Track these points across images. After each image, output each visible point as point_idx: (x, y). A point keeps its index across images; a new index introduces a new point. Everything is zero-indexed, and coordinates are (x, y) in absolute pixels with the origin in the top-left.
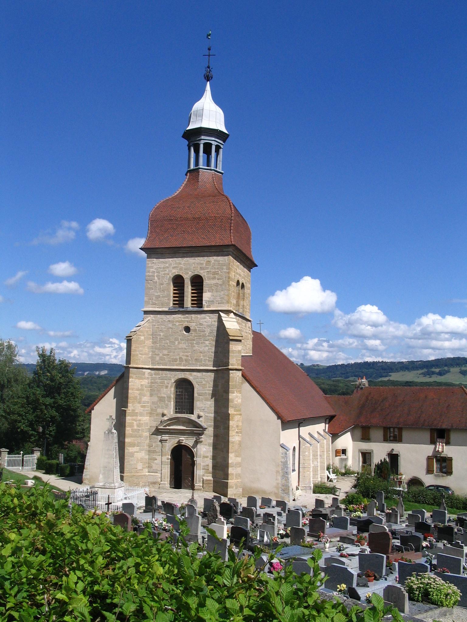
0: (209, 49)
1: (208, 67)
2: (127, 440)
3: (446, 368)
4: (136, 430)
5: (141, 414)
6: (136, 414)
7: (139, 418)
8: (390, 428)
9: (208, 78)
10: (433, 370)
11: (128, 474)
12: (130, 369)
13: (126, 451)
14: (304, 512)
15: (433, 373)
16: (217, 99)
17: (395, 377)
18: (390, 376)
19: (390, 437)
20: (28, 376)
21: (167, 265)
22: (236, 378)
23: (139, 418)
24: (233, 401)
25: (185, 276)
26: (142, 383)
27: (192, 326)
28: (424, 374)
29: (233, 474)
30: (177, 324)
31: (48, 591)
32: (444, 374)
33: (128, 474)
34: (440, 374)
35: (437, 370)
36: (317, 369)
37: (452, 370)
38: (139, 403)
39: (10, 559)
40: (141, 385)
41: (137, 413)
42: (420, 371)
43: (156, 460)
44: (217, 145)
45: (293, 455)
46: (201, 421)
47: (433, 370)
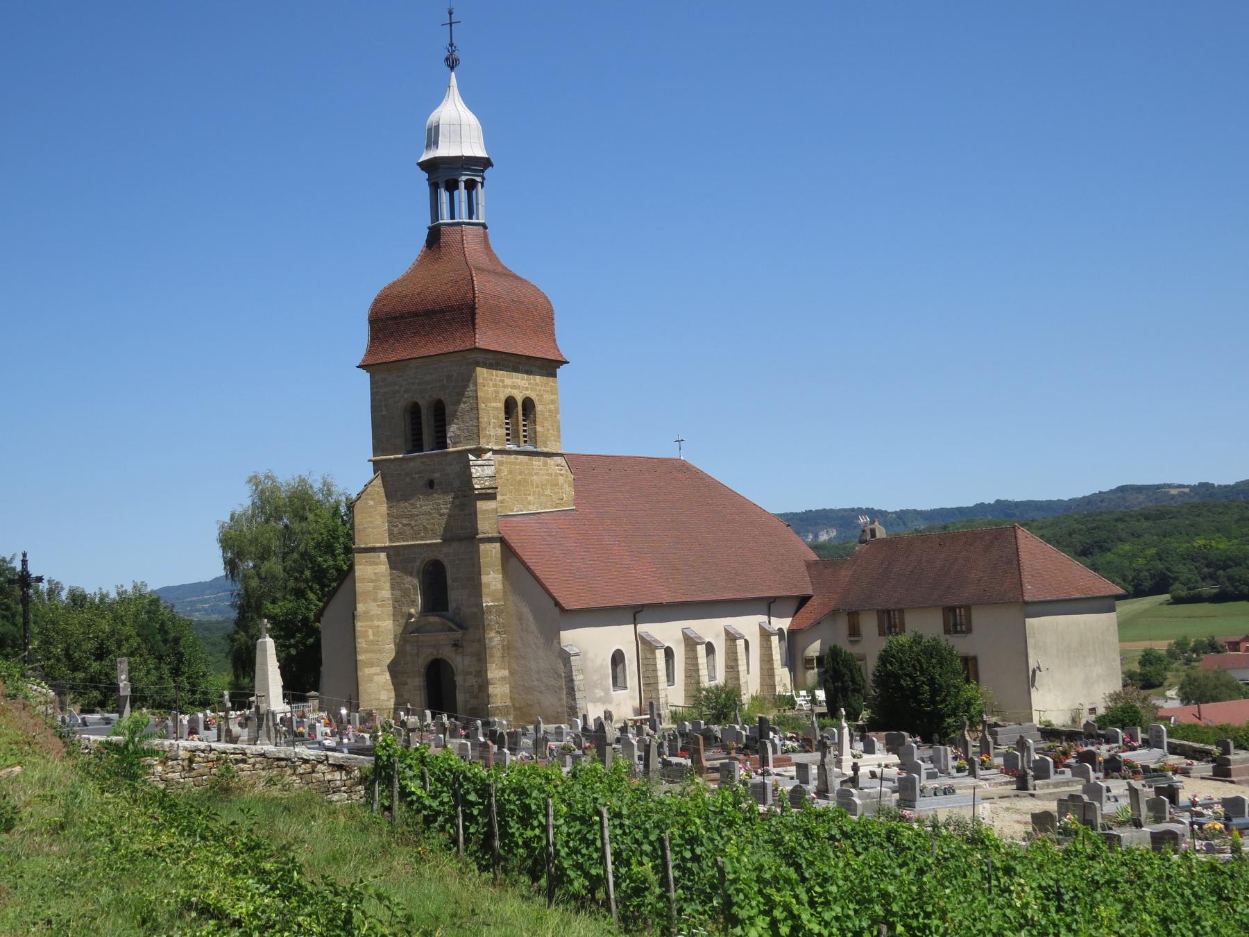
0: (451, 13)
1: (451, 45)
2: (359, 658)
4: (372, 641)
7: (376, 623)
8: (888, 612)
9: (452, 63)
11: (1235, 767)
12: (482, 547)
13: (360, 674)
14: (310, 704)
19: (890, 628)
21: (397, 388)
22: (491, 551)
23: (376, 623)
24: (488, 585)
25: (422, 403)
26: (376, 571)
27: (437, 475)
29: (496, 695)
30: (417, 476)
33: (1235, 767)
38: (375, 600)
39: (921, 920)
40: (375, 573)
41: (373, 615)
43: (407, 684)
44: (467, 180)
45: (727, 667)
46: (717, 636)
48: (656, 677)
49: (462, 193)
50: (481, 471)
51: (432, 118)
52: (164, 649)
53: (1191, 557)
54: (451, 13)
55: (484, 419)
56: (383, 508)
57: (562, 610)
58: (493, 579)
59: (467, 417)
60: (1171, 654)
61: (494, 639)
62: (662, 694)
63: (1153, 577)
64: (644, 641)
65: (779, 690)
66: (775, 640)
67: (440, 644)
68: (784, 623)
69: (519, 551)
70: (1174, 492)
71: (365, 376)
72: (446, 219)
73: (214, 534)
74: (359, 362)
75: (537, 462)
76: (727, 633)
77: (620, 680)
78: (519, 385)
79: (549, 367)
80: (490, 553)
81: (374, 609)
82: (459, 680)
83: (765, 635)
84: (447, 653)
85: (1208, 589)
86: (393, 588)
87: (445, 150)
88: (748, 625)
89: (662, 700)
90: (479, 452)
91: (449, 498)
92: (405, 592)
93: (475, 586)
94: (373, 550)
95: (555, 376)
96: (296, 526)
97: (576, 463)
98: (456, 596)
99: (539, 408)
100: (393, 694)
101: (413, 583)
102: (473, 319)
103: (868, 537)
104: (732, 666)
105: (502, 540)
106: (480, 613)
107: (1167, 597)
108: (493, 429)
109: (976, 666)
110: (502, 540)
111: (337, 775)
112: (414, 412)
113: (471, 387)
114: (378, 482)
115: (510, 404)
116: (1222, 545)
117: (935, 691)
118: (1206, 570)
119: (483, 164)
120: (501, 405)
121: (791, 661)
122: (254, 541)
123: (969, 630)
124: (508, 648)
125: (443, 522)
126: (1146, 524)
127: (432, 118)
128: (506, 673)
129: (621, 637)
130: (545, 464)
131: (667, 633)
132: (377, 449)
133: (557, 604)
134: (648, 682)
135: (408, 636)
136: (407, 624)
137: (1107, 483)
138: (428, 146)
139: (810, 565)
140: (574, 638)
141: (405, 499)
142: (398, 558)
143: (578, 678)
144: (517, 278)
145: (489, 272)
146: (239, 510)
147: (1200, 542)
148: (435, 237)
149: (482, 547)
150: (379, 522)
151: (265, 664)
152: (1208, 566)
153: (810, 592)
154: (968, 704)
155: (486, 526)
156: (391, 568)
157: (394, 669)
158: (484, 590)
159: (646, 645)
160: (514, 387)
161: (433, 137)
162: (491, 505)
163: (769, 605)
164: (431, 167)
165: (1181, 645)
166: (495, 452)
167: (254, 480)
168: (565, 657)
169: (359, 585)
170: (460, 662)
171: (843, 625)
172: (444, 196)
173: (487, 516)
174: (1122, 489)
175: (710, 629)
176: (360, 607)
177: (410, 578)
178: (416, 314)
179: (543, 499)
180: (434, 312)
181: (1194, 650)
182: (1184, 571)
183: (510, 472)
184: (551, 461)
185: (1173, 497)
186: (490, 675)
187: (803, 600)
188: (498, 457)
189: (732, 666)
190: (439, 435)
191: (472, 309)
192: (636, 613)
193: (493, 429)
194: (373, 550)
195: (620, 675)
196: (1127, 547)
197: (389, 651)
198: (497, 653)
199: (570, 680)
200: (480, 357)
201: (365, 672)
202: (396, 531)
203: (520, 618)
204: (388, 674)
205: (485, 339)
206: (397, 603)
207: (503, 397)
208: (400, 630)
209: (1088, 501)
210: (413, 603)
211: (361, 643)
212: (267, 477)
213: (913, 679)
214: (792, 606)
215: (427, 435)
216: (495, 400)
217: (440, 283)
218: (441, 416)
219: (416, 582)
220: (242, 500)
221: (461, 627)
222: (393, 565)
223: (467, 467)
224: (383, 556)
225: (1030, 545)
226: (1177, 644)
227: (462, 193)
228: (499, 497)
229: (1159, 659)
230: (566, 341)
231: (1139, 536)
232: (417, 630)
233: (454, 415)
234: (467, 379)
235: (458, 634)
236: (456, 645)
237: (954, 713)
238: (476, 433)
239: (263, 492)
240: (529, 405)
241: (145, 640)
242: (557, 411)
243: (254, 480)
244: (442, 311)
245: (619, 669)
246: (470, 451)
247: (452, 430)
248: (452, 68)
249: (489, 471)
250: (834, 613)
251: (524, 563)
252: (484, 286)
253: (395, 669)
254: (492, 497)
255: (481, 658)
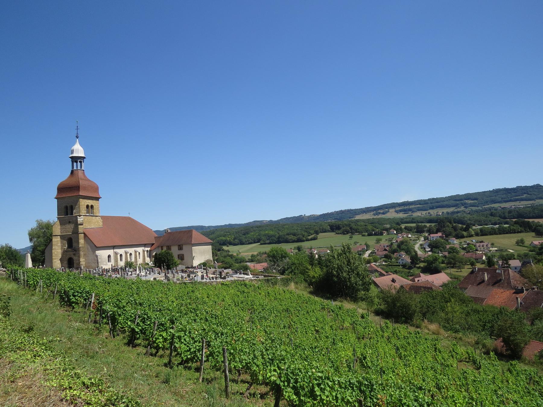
0: (77, 127)
2: (53, 258)
3: (387, 210)
5: (58, 249)
6: (56, 250)
9: (77, 137)
10: (380, 211)
12: (80, 235)
15: (380, 213)
16: (81, 145)
17: (358, 217)
18: (355, 217)
20: (286, 234)
25: (68, 206)
28: (374, 215)
31: (44, 237)
32: (386, 213)
34: (383, 213)
35: (382, 211)
36: (314, 217)
37: (390, 210)
42: (372, 213)
47: (380, 211)
48: (118, 260)
49: (79, 164)
50: (80, 220)
51: (72, 148)
52: (12, 258)
53: (265, 235)
54: (77, 127)
55: (81, 209)
56: (59, 227)
57: (96, 247)
58: (82, 241)
59: (77, 209)
60: (257, 255)
61: (82, 253)
62: (119, 263)
63: (257, 239)
64: (115, 253)
65: (146, 262)
66: (146, 252)
67: (71, 254)
68: (149, 249)
69: (88, 235)
70: (265, 222)
71: (56, 200)
72: (75, 168)
73: (27, 233)
74: (55, 197)
75: (93, 218)
76: (135, 251)
77: (110, 260)
78: (90, 202)
79: (97, 199)
80: (81, 236)
81: (57, 248)
82: (75, 261)
83: (144, 251)
84: (72, 256)
85: (268, 241)
86: (61, 243)
87: (75, 155)
88: (140, 249)
89: (119, 264)
90: (80, 216)
91: (73, 225)
92: (64, 244)
93: (78, 242)
94: (57, 235)
95: (99, 200)
96: (47, 231)
97: (102, 217)
98: (74, 245)
99: (94, 207)
100: (61, 265)
101: (65, 242)
102: (79, 189)
103: (167, 232)
104: (136, 258)
105: (84, 233)
106: (79, 248)
107: (259, 243)
108: (83, 211)
109: (184, 256)
110: (84, 233)
111: (4, 273)
112: (66, 207)
113: (79, 203)
114: (58, 222)
115: (88, 206)
116: (271, 233)
117: (168, 261)
118: (268, 238)
119: (84, 158)
120: (86, 206)
121: (150, 256)
122: (36, 234)
123: (183, 249)
124: (85, 255)
125: (72, 230)
126: (257, 228)
127: (72, 148)
128: (84, 260)
129: (111, 252)
130: (96, 218)
131: (121, 251)
132: (58, 215)
133: (95, 246)
134: (116, 261)
135: (64, 253)
136: (64, 251)
137: (251, 220)
138: (71, 154)
139: (155, 237)
140: (98, 252)
141: (64, 225)
142: (62, 237)
143: (99, 260)
144: (90, 181)
145: (83, 179)
146: (33, 227)
147: (267, 232)
148: (72, 172)
149: (80, 235)
150: (58, 230)
151: (28, 259)
152: (268, 237)
153: (154, 243)
154: (175, 263)
155: (80, 230)
156: (61, 239)
157: (61, 260)
158: (80, 243)
159: (116, 254)
160: (88, 203)
161: (72, 152)
162: (82, 226)
163: (145, 245)
164: (72, 158)
165: (260, 253)
166: (84, 216)
167: (37, 221)
168: (97, 256)
169: (53, 243)
170: (75, 258)
171: (160, 248)
172: (75, 164)
173: (81, 229)
174: (254, 221)
175: (131, 250)
176: (53, 247)
177: (64, 241)
178: (67, 188)
179: (95, 225)
180: (71, 187)
181: (262, 254)
182: (263, 238)
183: (87, 220)
184: (97, 217)
185: (264, 223)
186: (81, 260)
187: (153, 244)
188: (84, 217)
189: (136, 258)
190: (69, 213)
191: (79, 187)
192: (114, 247)
193: (83, 211)
194: (57, 235)
195: (110, 259)
196: (252, 233)
197: (60, 256)
198: (82, 256)
199: (98, 261)
200: (81, 197)
201: (54, 261)
202: (62, 232)
203: (88, 249)
204: (60, 261)
205: (81, 193)
206: (62, 246)
207: (86, 205)
208: (62, 252)
209: (247, 224)
210: (65, 246)
211: (53, 255)
212: (40, 220)
213: (164, 259)
214: (150, 246)
215: (69, 212)
216: (84, 205)
217: (73, 182)
218: (72, 208)
219: (66, 242)
220: (34, 225)
221: (75, 251)
222: (61, 238)
223: (77, 219)
224: (59, 237)
225: (195, 233)
226: (259, 253)
227: (79, 164)
228: (84, 225)
229: (255, 256)
230: (101, 193)
231: (255, 231)
232: (66, 252)
233: (75, 208)
234: (77, 201)
235: (75, 252)
236: (74, 254)
237: (172, 264)
238: (79, 212)
239: (39, 223)
240: (92, 207)
241: (7, 256)
242: (99, 207)
243: (37, 221)
244: (73, 187)
245: (110, 258)
246: (78, 216)
247: (74, 211)
248: (77, 138)
249: (81, 220)
250: (158, 247)
251: (88, 238)
252: (81, 183)
253: (61, 260)
254: (82, 225)
255: (79, 257)
